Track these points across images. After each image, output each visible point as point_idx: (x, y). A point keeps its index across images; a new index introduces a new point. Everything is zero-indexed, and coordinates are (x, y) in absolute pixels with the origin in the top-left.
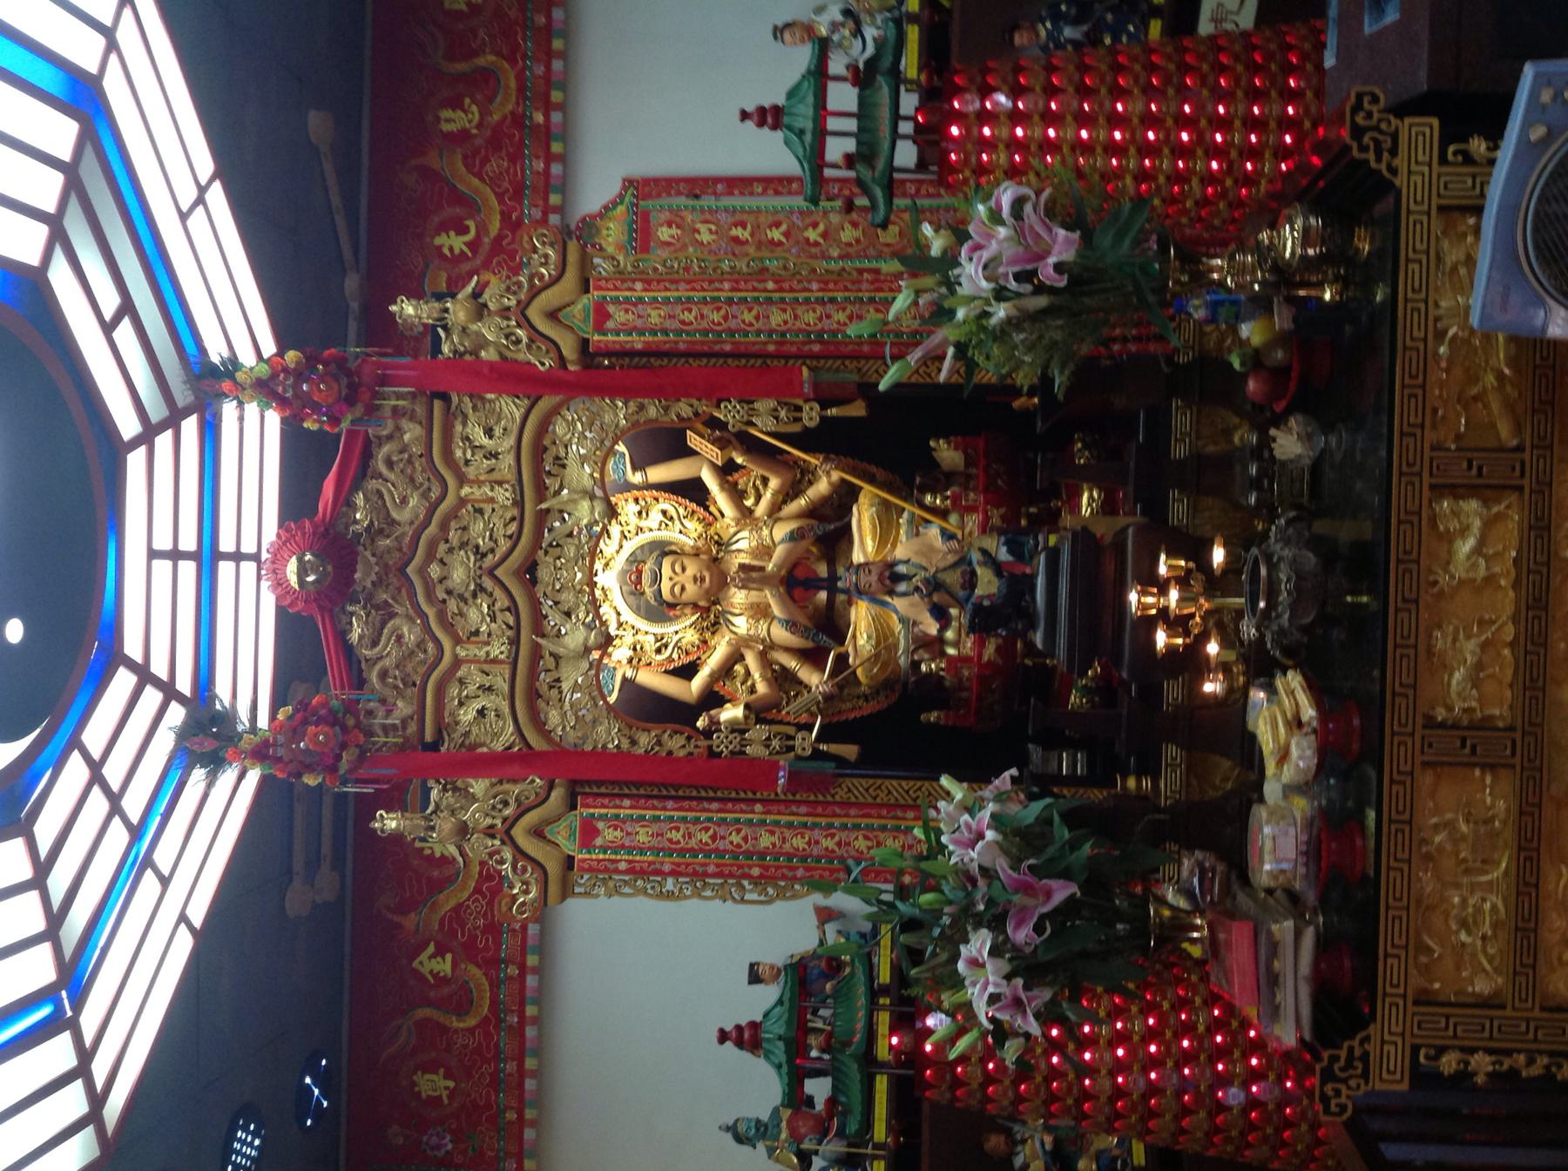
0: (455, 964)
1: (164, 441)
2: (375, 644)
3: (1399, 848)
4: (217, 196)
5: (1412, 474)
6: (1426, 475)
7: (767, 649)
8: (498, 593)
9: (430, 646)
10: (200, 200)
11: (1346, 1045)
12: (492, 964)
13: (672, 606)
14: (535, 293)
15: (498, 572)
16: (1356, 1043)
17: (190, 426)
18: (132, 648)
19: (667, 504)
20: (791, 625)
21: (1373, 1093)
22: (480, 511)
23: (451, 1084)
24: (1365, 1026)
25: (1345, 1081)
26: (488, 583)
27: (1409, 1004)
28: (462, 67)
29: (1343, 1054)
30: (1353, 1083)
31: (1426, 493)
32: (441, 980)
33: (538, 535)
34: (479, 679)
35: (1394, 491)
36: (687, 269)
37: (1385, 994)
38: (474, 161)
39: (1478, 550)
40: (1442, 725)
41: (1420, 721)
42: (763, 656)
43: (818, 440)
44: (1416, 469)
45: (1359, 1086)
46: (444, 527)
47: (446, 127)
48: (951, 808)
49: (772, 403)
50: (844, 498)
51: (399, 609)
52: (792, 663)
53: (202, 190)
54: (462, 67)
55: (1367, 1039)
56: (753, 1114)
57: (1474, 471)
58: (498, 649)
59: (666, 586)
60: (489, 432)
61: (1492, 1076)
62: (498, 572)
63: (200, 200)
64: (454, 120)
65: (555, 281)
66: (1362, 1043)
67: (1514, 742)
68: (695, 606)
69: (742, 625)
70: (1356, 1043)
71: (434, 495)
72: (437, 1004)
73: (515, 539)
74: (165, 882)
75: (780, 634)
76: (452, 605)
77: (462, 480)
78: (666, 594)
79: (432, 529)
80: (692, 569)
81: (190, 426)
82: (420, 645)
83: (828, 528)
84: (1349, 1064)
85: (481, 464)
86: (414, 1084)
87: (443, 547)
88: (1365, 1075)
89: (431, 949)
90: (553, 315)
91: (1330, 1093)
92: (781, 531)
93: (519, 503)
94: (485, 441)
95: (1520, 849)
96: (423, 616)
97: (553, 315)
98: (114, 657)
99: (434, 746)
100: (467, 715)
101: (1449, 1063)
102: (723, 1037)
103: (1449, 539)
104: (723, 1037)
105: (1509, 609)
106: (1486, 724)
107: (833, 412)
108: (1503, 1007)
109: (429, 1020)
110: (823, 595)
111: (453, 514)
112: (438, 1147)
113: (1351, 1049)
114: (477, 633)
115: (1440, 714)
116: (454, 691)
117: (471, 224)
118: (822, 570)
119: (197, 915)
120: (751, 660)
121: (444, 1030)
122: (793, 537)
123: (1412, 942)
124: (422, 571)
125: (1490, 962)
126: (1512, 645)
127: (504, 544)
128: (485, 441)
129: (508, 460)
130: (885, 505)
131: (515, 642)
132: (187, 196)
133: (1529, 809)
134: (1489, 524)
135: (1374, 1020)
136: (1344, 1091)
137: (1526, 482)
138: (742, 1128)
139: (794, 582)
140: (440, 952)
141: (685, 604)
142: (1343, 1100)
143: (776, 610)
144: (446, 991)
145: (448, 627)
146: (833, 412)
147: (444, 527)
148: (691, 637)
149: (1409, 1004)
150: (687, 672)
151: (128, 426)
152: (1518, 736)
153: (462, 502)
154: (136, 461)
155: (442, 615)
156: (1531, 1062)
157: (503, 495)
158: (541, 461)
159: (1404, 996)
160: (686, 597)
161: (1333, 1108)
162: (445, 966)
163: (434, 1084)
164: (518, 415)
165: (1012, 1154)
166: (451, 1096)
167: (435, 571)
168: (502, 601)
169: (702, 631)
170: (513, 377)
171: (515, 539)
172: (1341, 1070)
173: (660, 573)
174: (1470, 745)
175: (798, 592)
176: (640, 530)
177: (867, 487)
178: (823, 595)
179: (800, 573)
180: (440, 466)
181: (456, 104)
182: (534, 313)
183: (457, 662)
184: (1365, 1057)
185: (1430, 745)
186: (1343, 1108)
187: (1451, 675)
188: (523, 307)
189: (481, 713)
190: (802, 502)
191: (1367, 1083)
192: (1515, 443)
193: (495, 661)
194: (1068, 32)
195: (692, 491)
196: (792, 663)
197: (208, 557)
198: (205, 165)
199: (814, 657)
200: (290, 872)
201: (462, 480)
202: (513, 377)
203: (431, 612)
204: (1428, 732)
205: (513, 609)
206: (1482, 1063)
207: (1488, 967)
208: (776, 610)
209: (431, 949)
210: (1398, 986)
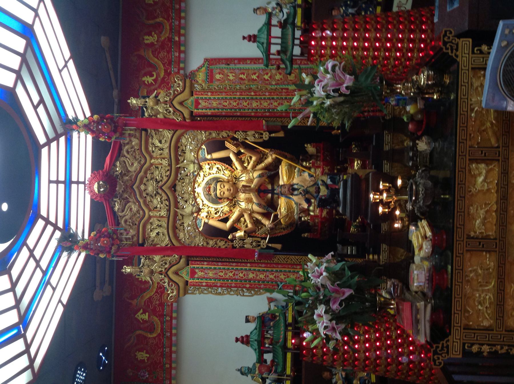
0: (149, 316)
1: (54, 145)
2: (123, 211)
3: (459, 278)
4: (71, 64)
5: (463, 155)
6: (467, 156)
7: (251, 213)
8: (163, 194)
9: (141, 212)
10: (66, 66)
11: (441, 343)
12: (161, 316)
13: (220, 199)
14: (175, 96)
15: (163, 188)
16: (444, 342)
17: (62, 140)
18: (43, 212)
19: (219, 165)
20: (259, 205)
21: (450, 358)
22: (157, 168)
23: (148, 355)
24: (448, 336)
25: (441, 354)
26: (160, 191)
27: (462, 329)
28: (151, 22)
29: (440, 346)
30: (443, 355)
31: (468, 162)
32: (145, 321)
33: (176, 175)
34: (157, 223)
35: (457, 161)
36: (225, 88)
37: (454, 326)
38: (155, 53)
39: (484, 180)
40: (473, 238)
41: (465, 236)
42: (250, 215)
43: (268, 144)
44: (464, 154)
45: (445, 356)
46: (146, 173)
47: (146, 42)
48: (312, 265)
49: (253, 132)
50: (277, 163)
51: (131, 200)
52: (260, 218)
53: (66, 62)
54: (151, 22)
55: (448, 341)
56: (247, 365)
57: (483, 155)
58: (163, 213)
59: (218, 192)
60: (160, 142)
61: (489, 353)
62: (163, 188)
63: (66, 66)
64: (149, 39)
65: (182, 92)
66: (446, 342)
67: (496, 243)
68: (228, 199)
69: (243, 205)
70: (444, 342)
71: (142, 162)
72: (143, 329)
73: (169, 177)
74: (54, 289)
75: (256, 208)
76: (148, 198)
77: (151, 157)
78: (218, 195)
79: (142, 173)
80: (227, 187)
81: (62, 140)
82: (138, 211)
83: (271, 173)
84: (442, 349)
85: (158, 152)
86: (136, 355)
87: (145, 179)
88: (448, 353)
89: (141, 311)
90: (181, 103)
91: (436, 358)
92: (256, 174)
93: (170, 165)
94: (159, 145)
95: (498, 278)
96: (139, 202)
97: (181, 103)
98: (37, 215)
99: (142, 245)
100: (153, 234)
101: (475, 349)
102: (237, 340)
103: (475, 177)
104: (237, 340)
105: (495, 200)
106: (487, 238)
107: (273, 135)
108: (493, 330)
109: (141, 334)
110: (270, 195)
111: (149, 169)
112: (144, 376)
113: (443, 344)
114: (156, 207)
115: (472, 234)
116: (149, 226)
117: (154, 73)
118: (270, 187)
119: (65, 300)
120: (246, 216)
121: (146, 338)
122: (260, 176)
123: (463, 309)
124: (138, 187)
125: (488, 316)
126: (496, 211)
127: (165, 179)
128: (159, 145)
129: (166, 151)
130: (290, 165)
131: (169, 210)
132: (61, 64)
133: (501, 265)
134: (488, 172)
135: (451, 334)
136: (441, 358)
137: (500, 158)
138: (243, 370)
139: (260, 191)
140: (144, 312)
141: (225, 198)
142: (440, 361)
143: (254, 200)
144: (146, 325)
145: (147, 206)
146: (273, 135)
147: (146, 173)
148: (226, 209)
149: (462, 329)
150: (225, 220)
151: (42, 140)
152: (498, 241)
153: (152, 165)
154: (44, 151)
155: (145, 202)
156: (502, 348)
157: (165, 162)
158: (178, 151)
159: (460, 327)
160: (225, 196)
161: (437, 363)
162: (146, 317)
163: (142, 356)
164: (170, 136)
165: (332, 379)
166: (148, 360)
167: (142, 187)
168: (165, 197)
169: (230, 207)
170: (168, 124)
171: (169, 177)
172: (440, 351)
173: (216, 188)
174: (482, 244)
175: (261, 194)
176: (210, 174)
177: (284, 160)
178: (270, 195)
179: (262, 188)
180: (144, 153)
181: (150, 34)
182: (175, 103)
183: (150, 217)
184: (447, 347)
185: (469, 244)
186: (440, 363)
187: (476, 221)
188: (171, 101)
189: (158, 234)
190: (263, 165)
191: (448, 355)
192: (496, 145)
193: (162, 217)
194: (350, 11)
195: (227, 161)
196: (260, 218)
197: (68, 183)
198: (67, 54)
199: (267, 215)
200: (95, 286)
201: (151, 157)
202: (168, 124)
203: (141, 201)
204: (468, 240)
205: (168, 200)
206: (486, 349)
207: (488, 317)
208: (254, 200)
209: (141, 311)
210: (458, 323)
